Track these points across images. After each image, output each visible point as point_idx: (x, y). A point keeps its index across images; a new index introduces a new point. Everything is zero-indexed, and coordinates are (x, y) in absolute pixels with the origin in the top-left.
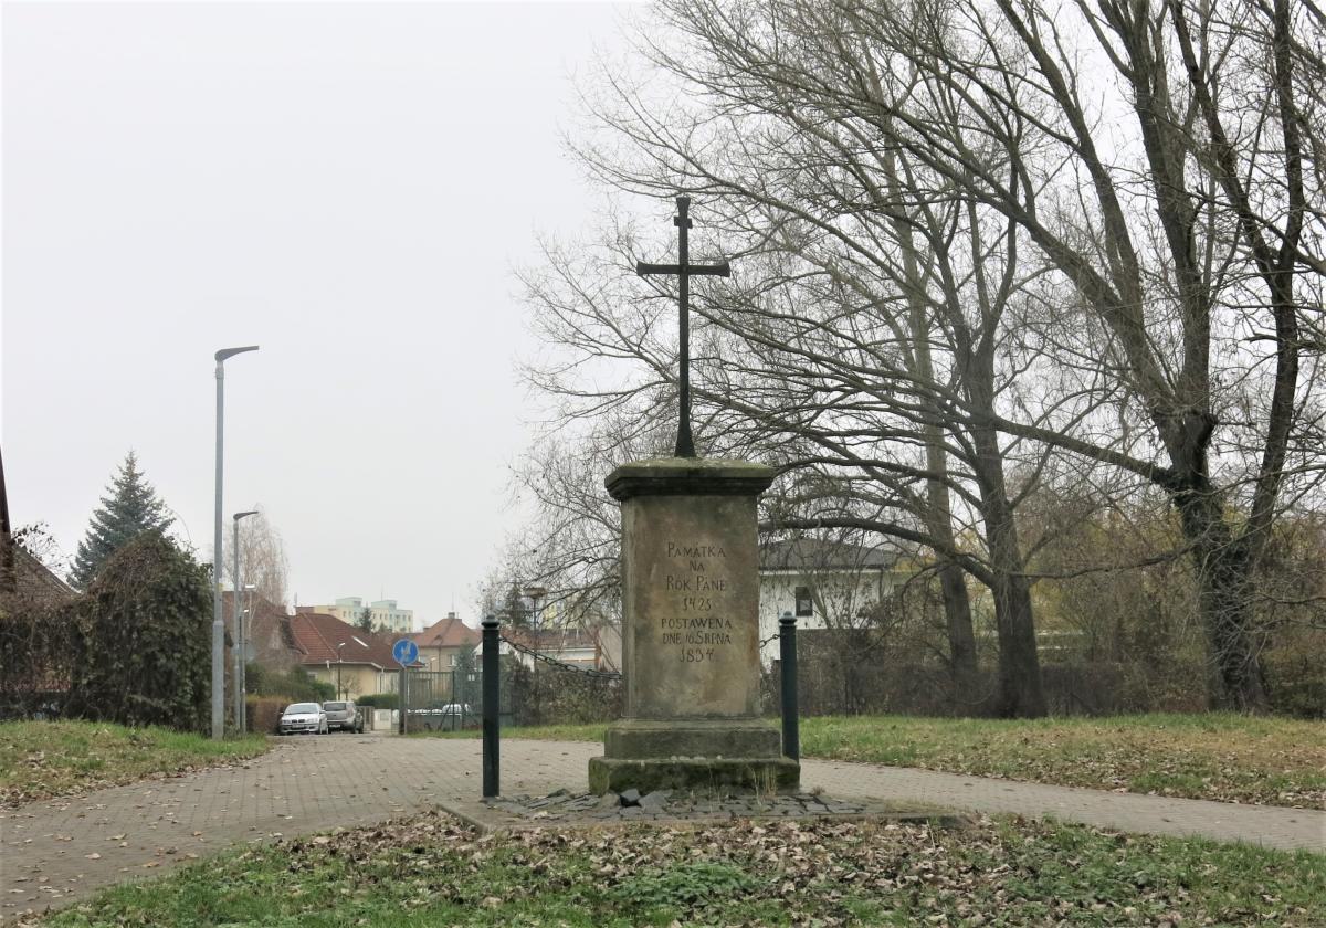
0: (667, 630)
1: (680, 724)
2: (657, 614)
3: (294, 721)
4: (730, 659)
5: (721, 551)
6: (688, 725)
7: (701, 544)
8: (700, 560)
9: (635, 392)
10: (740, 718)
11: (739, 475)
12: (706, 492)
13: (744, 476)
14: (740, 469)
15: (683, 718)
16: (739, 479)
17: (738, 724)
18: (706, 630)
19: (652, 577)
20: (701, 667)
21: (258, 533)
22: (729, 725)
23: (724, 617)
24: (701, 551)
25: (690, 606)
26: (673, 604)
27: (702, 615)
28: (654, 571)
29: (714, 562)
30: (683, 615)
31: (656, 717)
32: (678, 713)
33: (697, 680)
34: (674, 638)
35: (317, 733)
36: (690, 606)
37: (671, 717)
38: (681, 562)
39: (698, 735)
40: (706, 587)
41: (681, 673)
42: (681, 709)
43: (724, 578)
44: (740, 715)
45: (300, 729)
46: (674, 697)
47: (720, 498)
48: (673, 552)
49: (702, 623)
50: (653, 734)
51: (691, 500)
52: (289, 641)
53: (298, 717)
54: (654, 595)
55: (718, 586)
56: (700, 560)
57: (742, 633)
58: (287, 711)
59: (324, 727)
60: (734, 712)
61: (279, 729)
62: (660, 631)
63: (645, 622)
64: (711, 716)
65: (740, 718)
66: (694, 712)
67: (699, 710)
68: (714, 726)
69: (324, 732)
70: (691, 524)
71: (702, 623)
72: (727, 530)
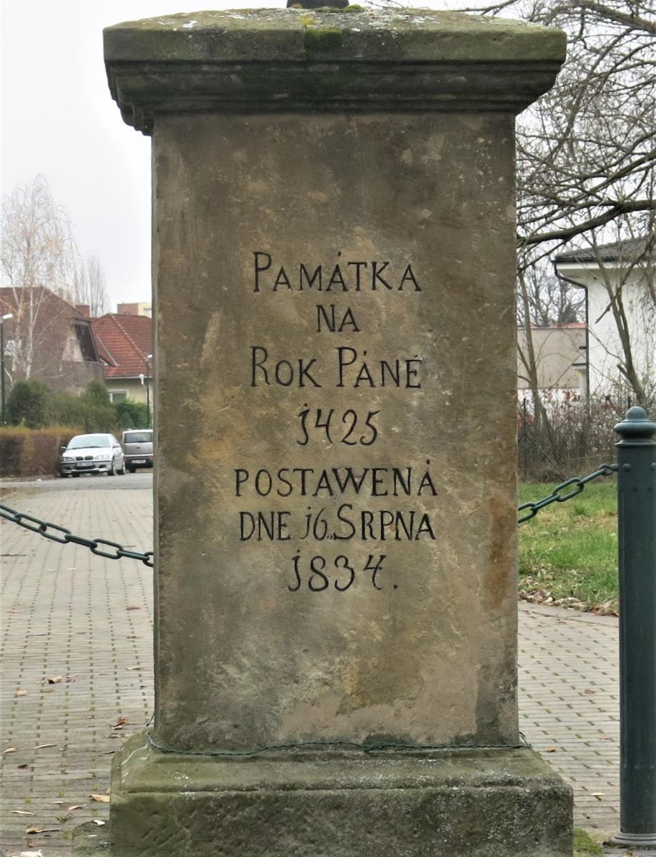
0: (251, 502)
1: (287, 772)
2: (220, 457)
3: (79, 459)
4: (434, 583)
5: (409, 275)
6: (304, 774)
7: (349, 255)
8: (343, 301)
9: (501, 7)
10: (462, 749)
11: (456, 54)
12: (355, 103)
13: (474, 54)
14: (458, 36)
15: (297, 752)
16: (461, 64)
17: (453, 770)
18: (364, 500)
19: (207, 350)
20: (349, 606)
21: (40, 212)
22: (426, 773)
23: (415, 465)
24: (348, 274)
25: (318, 435)
26: (268, 429)
27: (354, 458)
28: (211, 334)
29: (386, 305)
30: (296, 457)
31: (218, 749)
32: (281, 737)
33: (338, 644)
34: (270, 525)
35: (110, 473)
36: (318, 435)
37: (252, 746)
38: (289, 305)
39: (336, 805)
40: (365, 376)
41: (290, 622)
42: (289, 726)
43: (416, 351)
44: (458, 741)
45: (84, 470)
46: (270, 692)
47: (405, 120)
48: (269, 279)
49: (351, 480)
50: (201, 805)
51: (318, 126)
52: (90, 351)
53: (83, 453)
54: (212, 403)
55: (396, 373)
56: (343, 301)
57: (466, 508)
58: (72, 444)
59: (120, 465)
60: (443, 735)
61: (61, 470)
62: (230, 506)
63: (186, 478)
64: (380, 746)
65: (462, 749)
66: (330, 734)
67: (341, 726)
68: (382, 776)
69: (120, 472)
70: (322, 196)
71: (351, 480)
72: (426, 213)
